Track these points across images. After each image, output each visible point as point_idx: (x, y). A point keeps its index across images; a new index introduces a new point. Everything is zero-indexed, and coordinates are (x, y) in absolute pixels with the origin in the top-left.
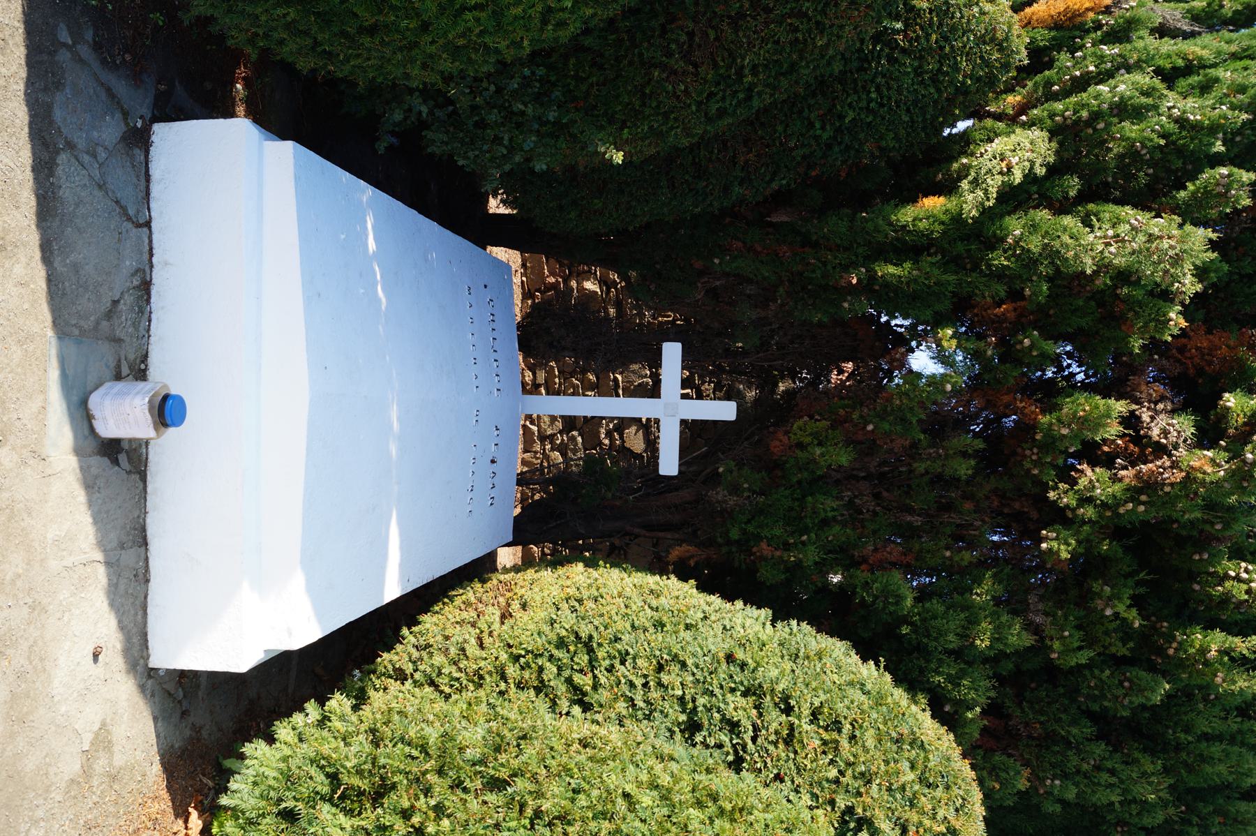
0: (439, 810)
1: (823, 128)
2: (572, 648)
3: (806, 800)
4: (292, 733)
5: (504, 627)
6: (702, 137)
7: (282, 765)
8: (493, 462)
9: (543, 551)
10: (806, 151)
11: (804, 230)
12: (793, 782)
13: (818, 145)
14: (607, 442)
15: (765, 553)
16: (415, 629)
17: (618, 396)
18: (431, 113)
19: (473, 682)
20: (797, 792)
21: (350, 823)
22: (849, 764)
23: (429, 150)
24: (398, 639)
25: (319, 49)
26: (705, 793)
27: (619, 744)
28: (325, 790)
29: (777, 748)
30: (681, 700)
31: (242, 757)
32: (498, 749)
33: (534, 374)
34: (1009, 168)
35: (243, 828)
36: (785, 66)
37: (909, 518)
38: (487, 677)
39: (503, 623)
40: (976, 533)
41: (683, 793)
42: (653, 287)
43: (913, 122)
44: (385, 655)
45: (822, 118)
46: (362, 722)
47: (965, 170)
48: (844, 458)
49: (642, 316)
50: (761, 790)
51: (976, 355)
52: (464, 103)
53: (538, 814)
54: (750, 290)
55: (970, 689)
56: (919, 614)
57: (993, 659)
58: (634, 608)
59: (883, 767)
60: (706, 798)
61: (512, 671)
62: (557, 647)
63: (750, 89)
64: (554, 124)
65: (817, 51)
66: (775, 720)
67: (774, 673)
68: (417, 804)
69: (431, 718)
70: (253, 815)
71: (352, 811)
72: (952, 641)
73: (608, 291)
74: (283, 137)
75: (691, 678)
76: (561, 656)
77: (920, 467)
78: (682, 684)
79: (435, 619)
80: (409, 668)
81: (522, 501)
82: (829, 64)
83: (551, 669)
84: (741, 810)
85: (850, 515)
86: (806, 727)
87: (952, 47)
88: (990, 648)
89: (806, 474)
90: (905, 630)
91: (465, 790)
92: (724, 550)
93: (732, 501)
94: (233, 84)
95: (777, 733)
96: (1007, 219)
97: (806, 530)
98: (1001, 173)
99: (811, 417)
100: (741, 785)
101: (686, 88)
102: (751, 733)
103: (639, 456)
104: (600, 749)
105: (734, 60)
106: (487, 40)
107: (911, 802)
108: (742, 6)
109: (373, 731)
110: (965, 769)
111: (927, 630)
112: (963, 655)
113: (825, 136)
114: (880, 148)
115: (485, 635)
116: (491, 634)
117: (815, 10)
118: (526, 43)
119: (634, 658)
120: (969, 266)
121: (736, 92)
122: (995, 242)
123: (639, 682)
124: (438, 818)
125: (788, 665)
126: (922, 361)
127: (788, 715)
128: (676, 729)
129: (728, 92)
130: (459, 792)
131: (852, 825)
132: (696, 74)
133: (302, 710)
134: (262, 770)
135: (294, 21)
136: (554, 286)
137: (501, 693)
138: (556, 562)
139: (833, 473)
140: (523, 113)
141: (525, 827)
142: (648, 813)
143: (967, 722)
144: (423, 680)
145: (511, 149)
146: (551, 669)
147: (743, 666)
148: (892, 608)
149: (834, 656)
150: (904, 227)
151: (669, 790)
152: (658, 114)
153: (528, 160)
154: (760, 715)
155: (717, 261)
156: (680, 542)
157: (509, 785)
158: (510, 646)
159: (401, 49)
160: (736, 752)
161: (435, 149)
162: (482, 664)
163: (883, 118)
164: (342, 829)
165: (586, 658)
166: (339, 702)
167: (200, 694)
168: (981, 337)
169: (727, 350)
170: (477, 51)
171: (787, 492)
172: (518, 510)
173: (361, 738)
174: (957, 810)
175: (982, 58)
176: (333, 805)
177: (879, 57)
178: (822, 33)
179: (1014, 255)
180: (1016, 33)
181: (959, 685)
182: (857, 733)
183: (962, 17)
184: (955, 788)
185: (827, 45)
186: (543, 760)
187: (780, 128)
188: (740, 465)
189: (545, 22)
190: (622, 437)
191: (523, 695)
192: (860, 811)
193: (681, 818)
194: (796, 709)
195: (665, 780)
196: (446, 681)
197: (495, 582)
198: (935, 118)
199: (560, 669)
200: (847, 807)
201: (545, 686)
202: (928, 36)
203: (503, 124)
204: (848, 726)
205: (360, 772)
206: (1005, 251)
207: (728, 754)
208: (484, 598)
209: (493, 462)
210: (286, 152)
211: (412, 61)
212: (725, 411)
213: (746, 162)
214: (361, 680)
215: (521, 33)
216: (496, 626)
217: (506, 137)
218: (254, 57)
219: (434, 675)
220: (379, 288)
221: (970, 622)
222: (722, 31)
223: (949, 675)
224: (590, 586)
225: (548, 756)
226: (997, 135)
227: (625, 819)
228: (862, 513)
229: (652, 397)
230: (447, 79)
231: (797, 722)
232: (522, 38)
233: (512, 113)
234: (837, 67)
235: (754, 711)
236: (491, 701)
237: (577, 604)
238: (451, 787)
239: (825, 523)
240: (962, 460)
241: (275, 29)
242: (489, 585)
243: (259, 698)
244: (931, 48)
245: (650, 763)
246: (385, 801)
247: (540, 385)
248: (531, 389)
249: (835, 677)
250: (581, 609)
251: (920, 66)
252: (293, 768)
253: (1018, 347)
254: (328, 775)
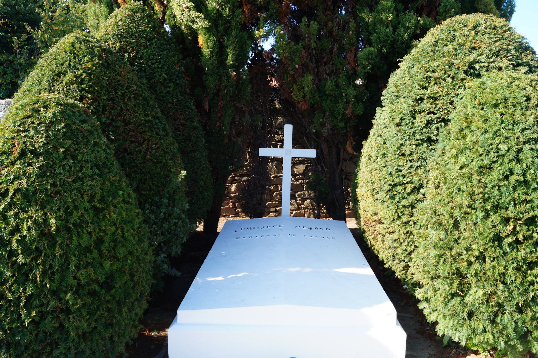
0: (468, 249)
1: (170, 87)
2: (395, 193)
3: (461, 91)
4: (432, 314)
5: (385, 222)
6: (174, 138)
7: (448, 318)
8: (311, 229)
9: (347, 209)
10: (179, 94)
11: (212, 96)
12: (453, 97)
13: (176, 89)
14: (300, 181)
15: (350, 111)
16: (385, 262)
17: (281, 176)
18: (164, 253)
19: (409, 236)
20: (458, 95)
21: (474, 288)
22: (445, 73)
23: (180, 254)
24: (390, 269)
25: (139, 298)
26: (459, 134)
27: (438, 172)
28: (459, 299)
29: (438, 104)
30: (417, 145)
31: (444, 335)
32: (441, 224)
33: (272, 212)
34: (187, 8)
35: (476, 335)
36: (145, 102)
37: (335, 50)
38: (407, 230)
39: (383, 223)
40: (342, 20)
41: (460, 144)
42: (236, 160)
43: (167, 49)
44: (397, 274)
45: (165, 88)
46: (428, 283)
47: (186, 26)
48: (309, 78)
49: (246, 166)
50: (457, 110)
51: (265, 20)
52: (161, 239)
53: (470, 206)
54: (237, 119)
55: (410, 22)
56: (377, 44)
57: (397, 12)
58: (376, 166)
59: (446, 58)
60: (462, 134)
61: (405, 219)
62: (394, 199)
63: (154, 117)
64: (169, 200)
65: (138, 89)
66: (426, 105)
67: (405, 106)
68: (465, 259)
69: (426, 253)
70: (470, 331)
71: (468, 287)
72: (389, 30)
73: (236, 180)
74: (175, 314)
75: (408, 141)
76: (398, 198)
77: (313, 45)
78: (410, 145)
79: (381, 253)
80: (403, 264)
81: (326, 217)
82: (143, 84)
83: (404, 202)
84: (466, 119)
85: (334, 75)
86: (429, 91)
87: (135, 33)
88: (392, 13)
89: (316, 94)
90: (384, 50)
91: (459, 238)
92: (349, 129)
93: (328, 126)
94: (152, 337)
95: (432, 104)
96: (209, 8)
97: (341, 94)
98: (189, 11)
99: (292, 92)
100: (456, 119)
101: (154, 144)
102: (432, 115)
103: (307, 167)
104: (440, 180)
105: (142, 124)
106: (136, 227)
107: (461, 46)
108: (120, 121)
109: (432, 279)
110: (446, 24)
111: (384, 41)
112: (395, 25)
113: (173, 86)
114: (178, 63)
115: (389, 231)
116: (389, 228)
117: (121, 89)
118: (137, 211)
119: (399, 166)
120: (229, 25)
121: (156, 123)
122: (219, 14)
123: (409, 164)
124: (472, 250)
125: (402, 100)
126: (267, 45)
127: (424, 99)
128: (430, 147)
129: (155, 126)
130: (460, 241)
131: (472, 71)
132: (148, 140)
133: (422, 310)
134: (449, 327)
135: (128, 309)
136: (234, 203)
137: (414, 223)
138: (356, 201)
139: (316, 82)
140: (165, 214)
141: (476, 212)
142: (469, 158)
143: (424, 23)
144: (409, 258)
145: (180, 218)
146: (404, 202)
147: (402, 119)
148: (374, 56)
149: (397, 80)
150: (211, 53)
151: (459, 150)
152: (165, 156)
153: (183, 212)
154: (424, 111)
155: (225, 133)
156: (345, 149)
157: (456, 219)
158: (394, 220)
159: (139, 264)
160: (440, 122)
161: (179, 251)
162: (401, 232)
163: (165, 62)
164: (476, 292)
165: (399, 187)
166: (419, 294)
167: (415, 354)
168: (258, 19)
169: (262, 129)
170: (140, 232)
171: (324, 102)
172: (331, 219)
173: (435, 283)
174: (465, 26)
175: (140, 20)
176: (465, 296)
177: (140, 63)
178: (131, 87)
179: (224, 5)
180: (129, 6)
181: (408, 27)
182: (431, 69)
183: (123, 29)
184: (455, 27)
185: (136, 85)
186: (445, 204)
187: (170, 105)
188: (312, 122)
189: (128, 203)
190: (298, 175)
191: (416, 214)
192: (466, 68)
193: (471, 145)
194: (421, 96)
195: (454, 152)
196: (409, 247)
197: (365, 227)
198: (165, 40)
199: (403, 198)
200: (464, 73)
201: (411, 205)
202: (131, 43)
203: (169, 222)
204: (428, 73)
205: (451, 284)
206: (223, 9)
207: (441, 125)
208: (372, 231)
209: (311, 229)
210: (181, 312)
211: (144, 259)
212: (288, 129)
213: (183, 119)
214: (408, 285)
215: (133, 213)
216: (384, 226)
217: (175, 221)
218: (142, 326)
219: (406, 253)
220: (238, 275)
221: (381, 23)
222: (130, 129)
223: (404, 31)
224: (367, 186)
225: (443, 202)
226: (172, 13)
227: (472, 169)
228: (333, 70)
229: (282, 162)
230: (151, 245)
231: (427, 95)
232: (135, 212)
233: (164, 218)
234: (144, 81)
235: (422, 114)
236: (418, 228)
237: (375, 191)
238: (458, 244)
239: (337, 86)
240: (311, 26)
241: (131, 317)
242: (366, 229)
243: (415, 329)
244: (136, 42)
245: (446, 158)
246: (464, 273)
247: (276, 210)
248: (278, 213)
249: (407, 79)
250: (377, 189)
251: (144, 46)
252: (449, 313)
253: (262, 3)
254: (452, 298)
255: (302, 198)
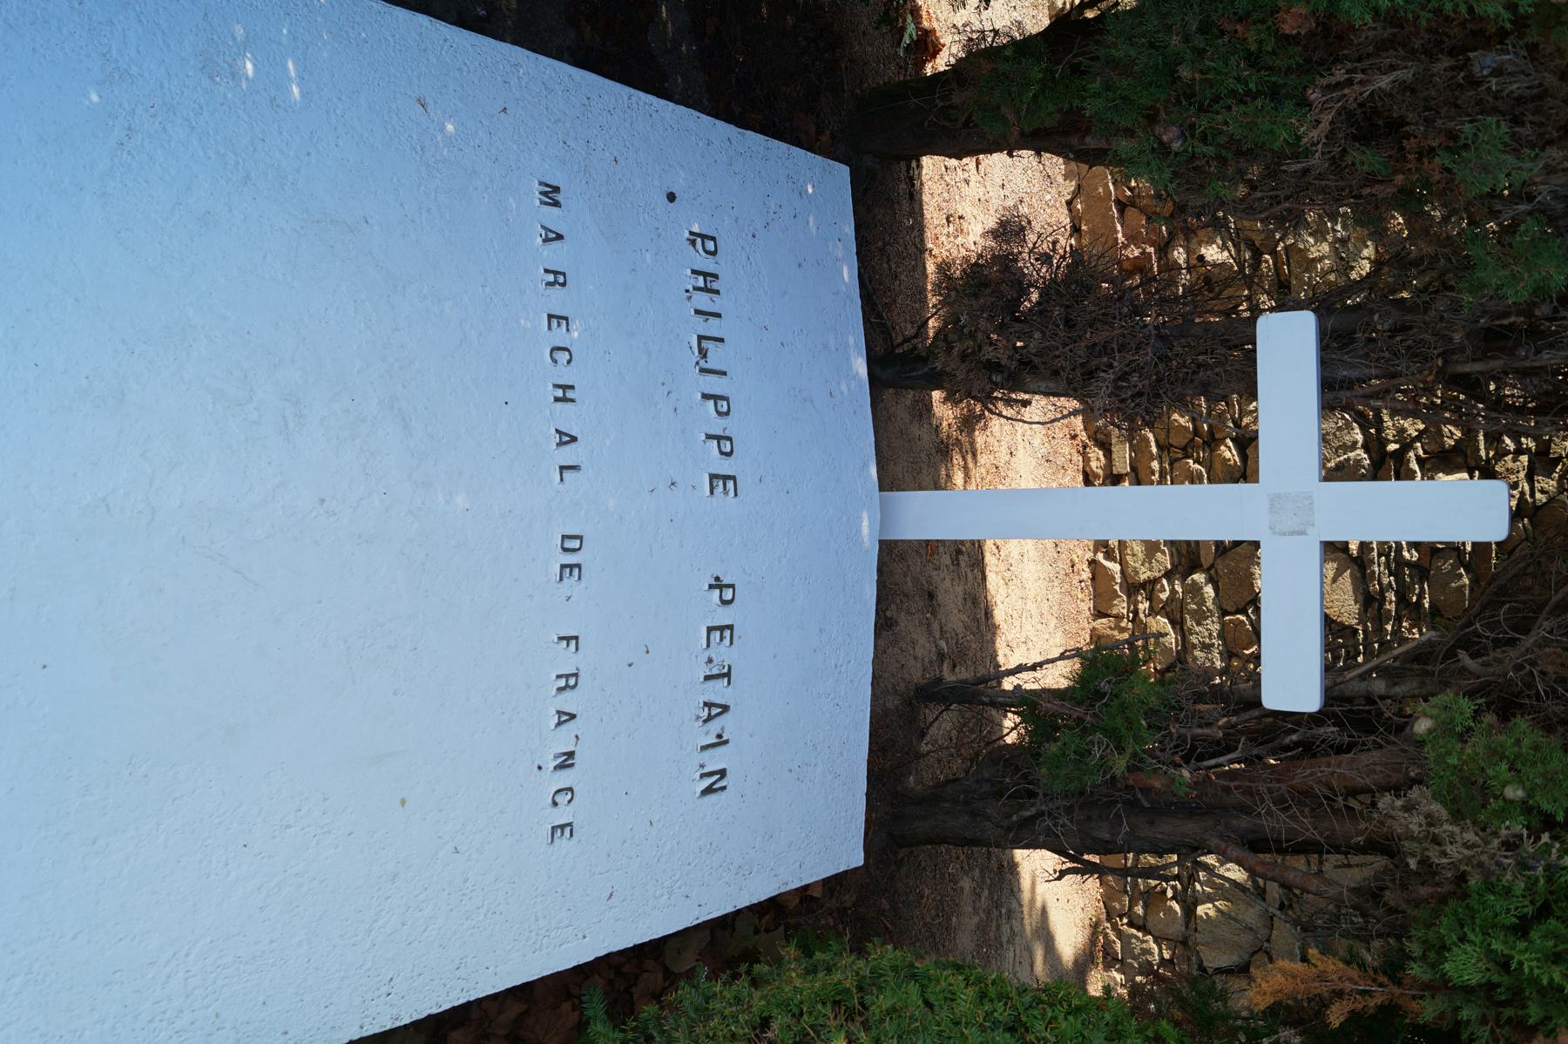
93: (1459, 845)
255: (1182, 605)
